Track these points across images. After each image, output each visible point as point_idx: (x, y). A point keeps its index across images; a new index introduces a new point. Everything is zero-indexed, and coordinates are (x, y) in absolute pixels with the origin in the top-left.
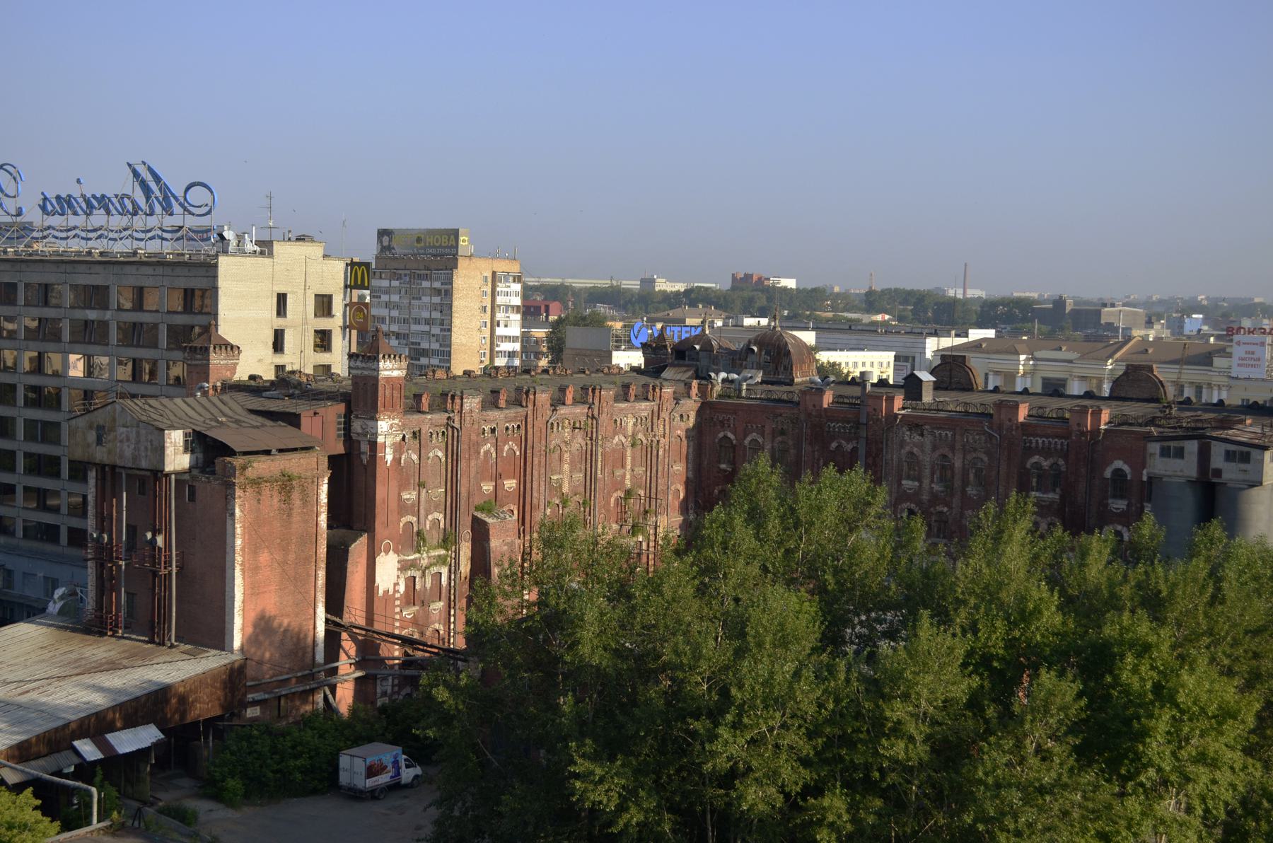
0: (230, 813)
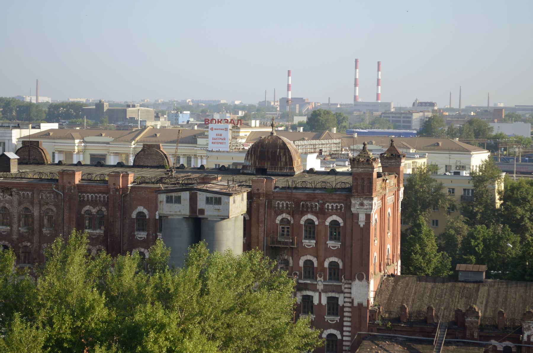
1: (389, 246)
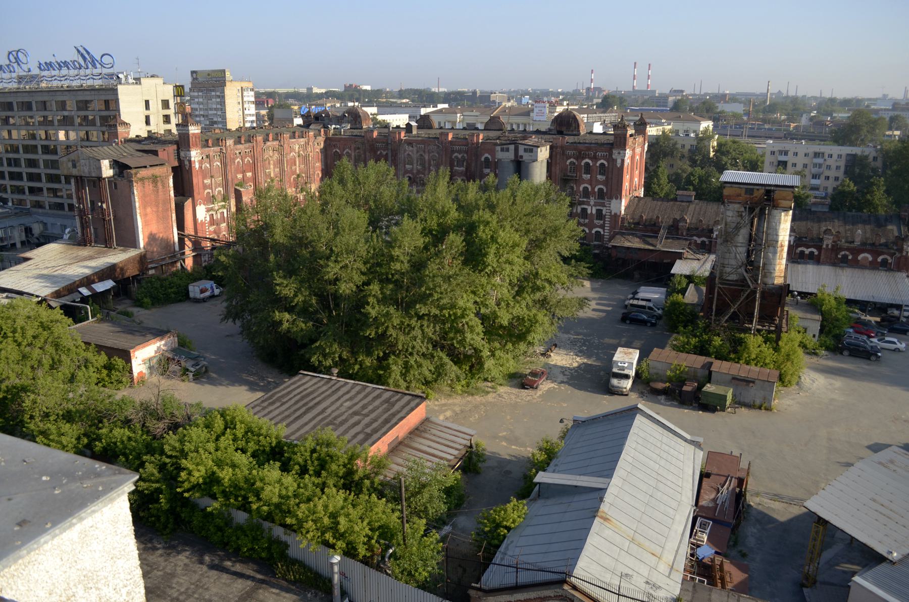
0: (147, 312)
1: (636, 179)
